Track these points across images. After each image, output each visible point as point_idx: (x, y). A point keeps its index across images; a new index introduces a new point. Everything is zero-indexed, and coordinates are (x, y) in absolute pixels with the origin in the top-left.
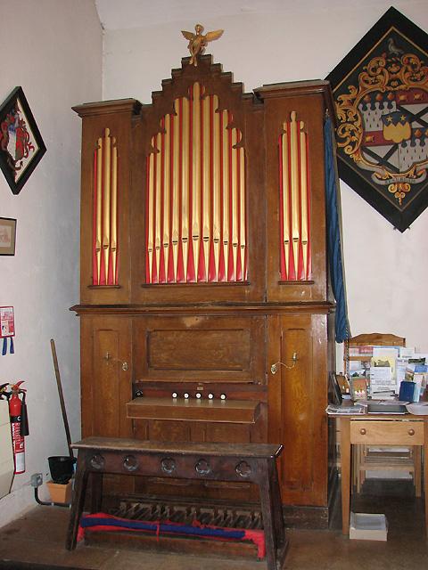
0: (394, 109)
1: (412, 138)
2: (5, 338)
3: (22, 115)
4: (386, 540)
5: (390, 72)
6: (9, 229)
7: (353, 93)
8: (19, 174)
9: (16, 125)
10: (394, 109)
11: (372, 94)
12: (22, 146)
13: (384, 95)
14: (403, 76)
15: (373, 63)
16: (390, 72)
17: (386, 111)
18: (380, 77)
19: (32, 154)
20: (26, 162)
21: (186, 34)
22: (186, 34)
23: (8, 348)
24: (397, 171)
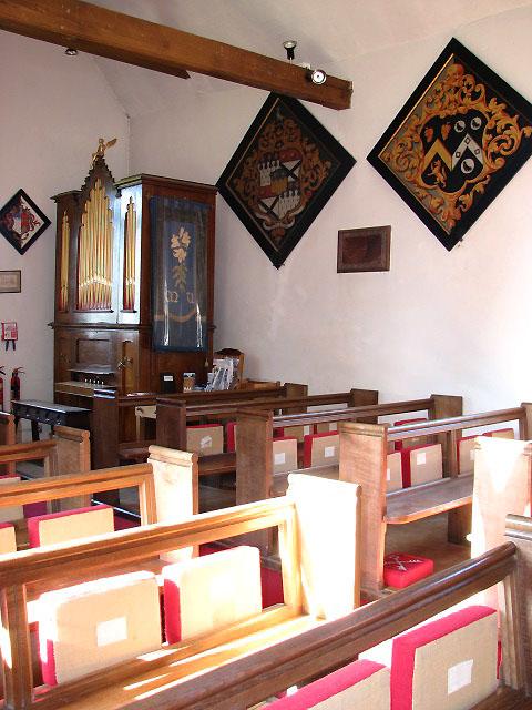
0: (278, 167)
1: (288, 190)
2: (8, 341)
3: (26, 205)
4: (500, 585)
5: (277, 136)
6: (15, 277)
7: (256, 155)
8: (25, 242)
9: (21, 212)
10: (278, 167)
11: (266, 155)
12: (26, 226)
13: (273, 155)
14: (284, 138)
15: (267, 130)
16: (277, 136)
17: (274, 169)
18: (271, 141)
19: (37, 228)
20: (31, 234)
21: (102, 141)
22: (102, 141)
23: (11, 344)
24: (276, 217)
